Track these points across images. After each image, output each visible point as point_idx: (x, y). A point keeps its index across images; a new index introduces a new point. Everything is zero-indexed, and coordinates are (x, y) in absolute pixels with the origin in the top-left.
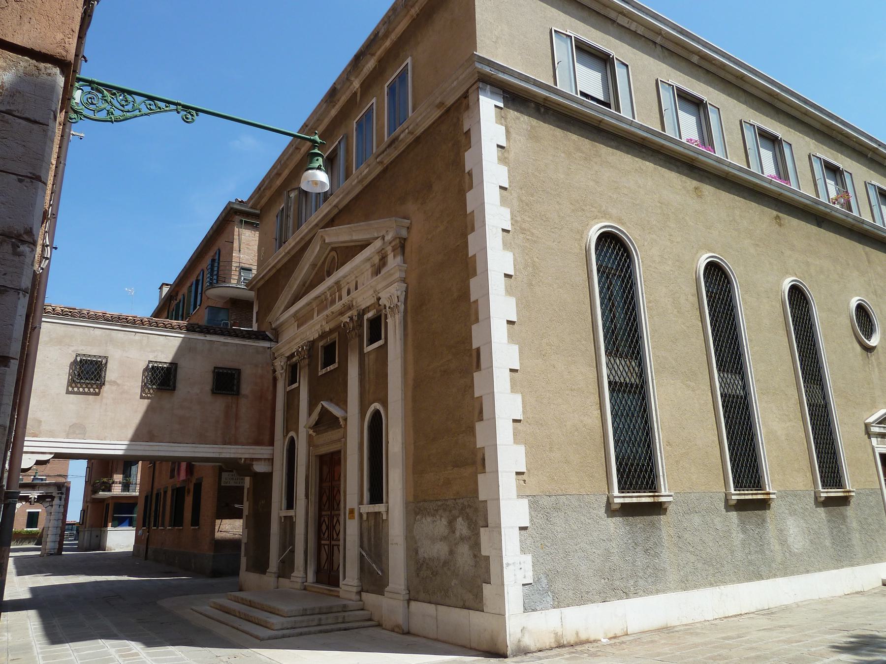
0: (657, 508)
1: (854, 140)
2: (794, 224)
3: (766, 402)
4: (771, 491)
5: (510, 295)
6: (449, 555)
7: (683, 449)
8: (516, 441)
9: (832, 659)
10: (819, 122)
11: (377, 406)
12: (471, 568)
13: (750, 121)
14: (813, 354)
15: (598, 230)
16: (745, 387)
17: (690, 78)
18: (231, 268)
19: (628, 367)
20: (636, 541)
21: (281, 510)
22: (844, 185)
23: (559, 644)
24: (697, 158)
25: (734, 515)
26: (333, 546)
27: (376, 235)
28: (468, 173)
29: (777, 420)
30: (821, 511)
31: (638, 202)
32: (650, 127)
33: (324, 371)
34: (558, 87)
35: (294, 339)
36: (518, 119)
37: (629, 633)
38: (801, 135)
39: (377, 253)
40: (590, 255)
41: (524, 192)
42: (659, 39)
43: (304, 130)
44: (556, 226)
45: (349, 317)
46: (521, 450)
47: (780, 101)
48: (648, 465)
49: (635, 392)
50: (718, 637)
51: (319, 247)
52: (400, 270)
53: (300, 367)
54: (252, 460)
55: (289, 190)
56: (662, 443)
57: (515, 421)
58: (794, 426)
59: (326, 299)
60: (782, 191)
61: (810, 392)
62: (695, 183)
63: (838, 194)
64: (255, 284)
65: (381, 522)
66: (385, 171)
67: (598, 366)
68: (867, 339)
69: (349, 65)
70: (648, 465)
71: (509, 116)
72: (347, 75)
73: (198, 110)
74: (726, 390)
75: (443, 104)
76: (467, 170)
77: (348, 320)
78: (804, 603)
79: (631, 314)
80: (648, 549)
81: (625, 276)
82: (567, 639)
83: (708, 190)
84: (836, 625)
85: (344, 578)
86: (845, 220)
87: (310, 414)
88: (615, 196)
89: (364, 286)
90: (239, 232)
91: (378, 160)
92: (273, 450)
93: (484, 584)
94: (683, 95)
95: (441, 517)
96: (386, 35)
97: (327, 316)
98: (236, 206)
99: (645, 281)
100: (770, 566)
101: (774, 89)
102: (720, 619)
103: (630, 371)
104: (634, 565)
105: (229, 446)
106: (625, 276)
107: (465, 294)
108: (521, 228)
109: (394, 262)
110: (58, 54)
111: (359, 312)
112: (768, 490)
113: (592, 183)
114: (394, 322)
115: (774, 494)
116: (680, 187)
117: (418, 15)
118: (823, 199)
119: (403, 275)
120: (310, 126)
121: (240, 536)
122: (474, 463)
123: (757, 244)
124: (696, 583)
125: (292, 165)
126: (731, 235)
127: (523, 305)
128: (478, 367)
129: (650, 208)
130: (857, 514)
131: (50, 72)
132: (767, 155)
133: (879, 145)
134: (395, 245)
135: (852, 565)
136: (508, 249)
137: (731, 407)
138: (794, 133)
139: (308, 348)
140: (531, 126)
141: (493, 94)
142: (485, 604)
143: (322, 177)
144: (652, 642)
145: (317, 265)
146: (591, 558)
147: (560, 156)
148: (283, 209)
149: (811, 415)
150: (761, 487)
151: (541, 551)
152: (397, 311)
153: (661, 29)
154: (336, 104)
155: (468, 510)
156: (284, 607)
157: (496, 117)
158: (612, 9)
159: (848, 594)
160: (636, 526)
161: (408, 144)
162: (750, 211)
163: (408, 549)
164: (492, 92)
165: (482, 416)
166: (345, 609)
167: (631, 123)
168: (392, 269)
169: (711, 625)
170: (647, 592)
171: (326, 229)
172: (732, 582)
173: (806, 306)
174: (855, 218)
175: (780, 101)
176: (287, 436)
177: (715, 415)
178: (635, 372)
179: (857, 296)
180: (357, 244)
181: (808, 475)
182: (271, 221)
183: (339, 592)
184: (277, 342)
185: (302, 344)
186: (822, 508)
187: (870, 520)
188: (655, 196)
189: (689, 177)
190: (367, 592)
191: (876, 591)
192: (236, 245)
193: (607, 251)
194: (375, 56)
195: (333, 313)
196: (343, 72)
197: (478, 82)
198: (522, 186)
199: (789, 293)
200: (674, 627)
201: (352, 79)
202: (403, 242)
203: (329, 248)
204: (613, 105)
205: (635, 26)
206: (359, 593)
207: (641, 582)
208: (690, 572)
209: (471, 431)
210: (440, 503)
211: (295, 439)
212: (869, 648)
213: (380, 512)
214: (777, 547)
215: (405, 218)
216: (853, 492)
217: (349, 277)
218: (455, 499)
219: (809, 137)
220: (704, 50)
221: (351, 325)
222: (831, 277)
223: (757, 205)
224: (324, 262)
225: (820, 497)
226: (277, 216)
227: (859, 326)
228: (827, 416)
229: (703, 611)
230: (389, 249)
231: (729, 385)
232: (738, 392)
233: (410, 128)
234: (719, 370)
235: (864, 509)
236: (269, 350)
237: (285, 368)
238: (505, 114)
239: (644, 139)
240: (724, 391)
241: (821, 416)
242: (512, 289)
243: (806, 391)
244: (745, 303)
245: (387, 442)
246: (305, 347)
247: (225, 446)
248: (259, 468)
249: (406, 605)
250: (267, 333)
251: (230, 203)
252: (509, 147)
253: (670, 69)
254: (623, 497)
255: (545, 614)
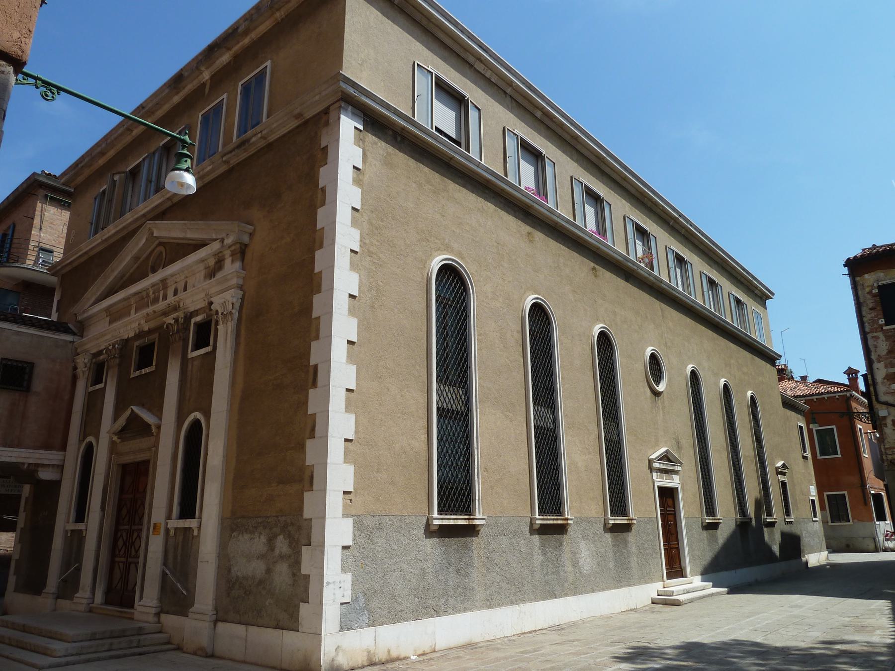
0: (471, 531)
1: (661, 208)
2: (607, 276)
3: (571, 436)
4: (569, 517)
5: (353, 316)
6: (266, 573)
7: (498, 475)
8: (347, 460)
9: (614, 668)
10: (635, 188)
11: (198, 415)
12: (289, 587)
13: (579, 178)
14: (613, 394)
15: (441, 261)
16: (555, 421)
17: (533, 131)
18: (28, 247)
19: (456, 395)
20: (449, 561)
21: (68, 523)
22: (649, 247)
23: (372, 662)
24: (532, 206)
25: (536, 538)
26: (130, 563)
27: (214, 237)
28: (322, 189)
29: (579, 452)
30: (608, 536)
31: (477, 239)
32: (494, 171)
33: (137, 373)
34: (416, 119)
35: (105, 335)
36: (376, 143)
37: (436, 650)
38: (619, 197)
39: (213, 255)
40: (431, 284)
41: (374, 216)
42: (509, 90)
43: (140, 112)
44: (402, 253)
45: (174, 319)
46: (350, 469)
47: (605, 164)
48: (466, 489)
49: (460, 420)
50: (517, 651)
51: (144, 241)
52: (238, 277)
53: (108, 366)
54: (37, 465)
55: (115, 172)
56: (480, 470)
57: (347, 440)
58: (592, 459)
59: (148, 296)
60: (600, 246)
61: (608, 428)
62: (528, 229)
63: (644, 254)
64: (59, 269)
65: (191, 538)
66: (230, 171)
67: (429, 392)
68: (656, 385)
69: (201, 54)
70: (466, 489)
71: (367, 139)
72: (197, 63)
73: (59, 89)
74: (539, 423)
75: (302, 115)
76: (320, 186)
77: (173, 322)
78: (589, 620)
79: (463, 345)
80: (459, 570)
81: (460, 308)
82: (379, 657)
83: (539, 236)
84: (615, 638)
85: (141, 598)
86: (647, 278)
87: (116, 417)
88: (457, 231)
89: (194, 288)
90: (42, 207)
91: (224, 159)
92: (65, 456)
93: (301, 603)
94: (526, 145)
95: (261, 534)
96: (246, 32)
97: (148, 314)
98: (41, 179)
99: (477, 315)
100: (563, 586)
101: (602, 153)
102: (518, 635)
103: (453, 398)
104: (446, 585)
105: (11, 449)
106: (460, 308)
107: (306, 309)
108: (369, 251)
109: (231, 267)
110: (14, 53)
111: (186, 314)
112: (566, 516)
113: (437, 216)
114: (225, 329)
115: (571, 519)
116: (515, 231)
117: (282, 20)
118: (632, 257)
119: (241, 282)
120: (147, 108)
121: (6, 552)
122: (301, 480)
123: (575, 291)
124: (500, 602)
125: (120, 146)
126: (554, 280)
127: (363, 327)
128: (314, 384)
129: (488, 246)
130: (636, 540)
131: (3, 70)
132: (590, 211)
133: (680, 216)
134: (235, 250)
135: (629, 586)
136: (354, 270)
137: (542, 438)
138: (614, 195)
139: (120, 346)
140: (387, 153)
141: (354, 116)
142: (301, 623)
143: (189, 179)
144: (458, 657)
145: (140, 259)
146: (408, 577)
147: (411, 185)
148: (104, 192)
149: (607, 449)
150: (561, 513)
151: (361, 570)
152: (230, 318)
153: (512, 81)
154: (181, 91)
155: (290, 528)
156: (70, 632)
157: (355, 138)
158: (471, 54)
159: (624, 611)
160: (451, 546)
161: (259, 148)
162: (573, 260)
163: (219, 567)
164: (353, 113)
165: (314, 434)
166: (140, 631)
167: (478, 165)
168: (229, 274)
169: (510, 641)
170: (456, 610)
171: (157, 222)
172: (531, 600)
173: (610, 351)
174: (655, 277)
175: (605, 164)
176: (84, 440)
177: (528, 445)
178: (462, 400)
179: (693, 364)
180: (190, 242)
181: (600, 504)
182: (88, 203)
183: (134, 613)
184: (82, 336)
185: (113, 342)
186: (610, 534)
187: (646, 546)
188: (493, 236)
189: (523, 222)
190: (167, 613)
191: (647, 608)
192: (37, 221)
193: (446, 282)
194: (230, 50)
195: (154, 312)
196: (193, 59)
197: (341, 101)
198: (373, 210)
199: (597, 339)
200: (477, 643)
201: (202, 69)
202: (243, 248)
203: (157, 242)
204: (723, 315)
205: (489, 74)
206: (158, 615)
207: (451, 601)
208: (495, 592)
209: (301, 447)
210: (260, 520)
211: (94, 444)
212: (643, 657)
213: (190, 528)
214: (569, 568)
215: (248, 223)
216: (635, 519)
217: (178, 276)
218: (277, 517)
219: (626, 201)
220: (547, 107)
221: (176, 328)
222: (632, 327)
223: (578, 255)
224: (148, 257)
225: (609, 524)
226: (95, 199)
227: (650, 372)
228: (620, 452)
229: (503, 628)
230: (227, 253)
231: (541, 418)
232: (549, 424)
233: (264, 132)
234: (534, 404)
235: (642, 535)
236: (71, 344)
237: (88, 365)
238: (364, 137)
239: (488, 181)
240: (537, 423)
241: (615, 451)
242: (355, 310)
243: (605, 428)
244: (561, 344)
245: (206, 454)
246: (117, 346)
247: (5, 449)
248: (45, 475)
249: (213, 626)
250: (69, 325)
251: (34, 174)
252: (365, 170)
253: (516, 119)
254: (442, 519)
255: (361, 633)
